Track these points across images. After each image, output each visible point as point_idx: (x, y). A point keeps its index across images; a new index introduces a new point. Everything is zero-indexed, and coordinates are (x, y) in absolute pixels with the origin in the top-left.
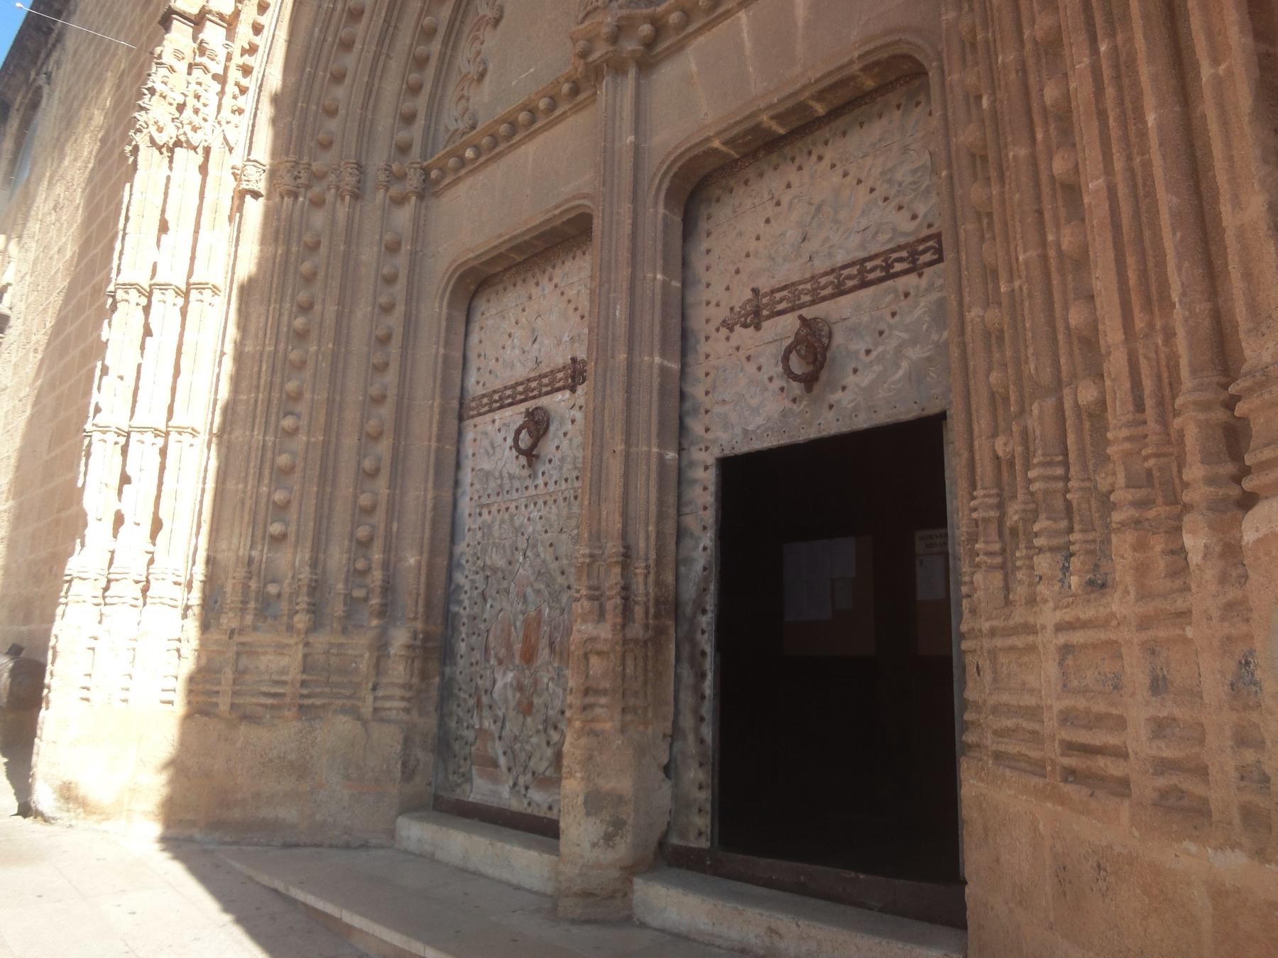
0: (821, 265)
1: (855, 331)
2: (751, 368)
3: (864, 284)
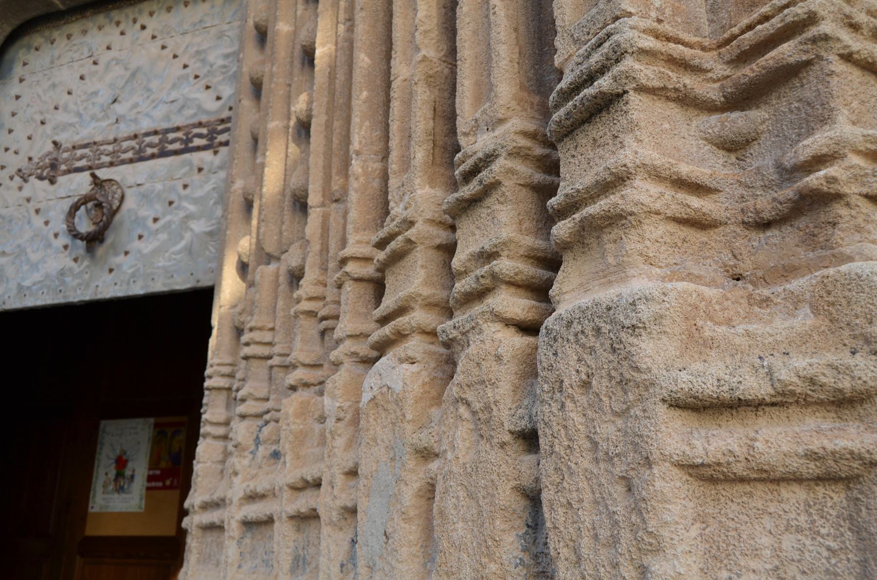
0: (125, 130)
1: (146, 198)
2: (38, 221)
3: (164, 154)
